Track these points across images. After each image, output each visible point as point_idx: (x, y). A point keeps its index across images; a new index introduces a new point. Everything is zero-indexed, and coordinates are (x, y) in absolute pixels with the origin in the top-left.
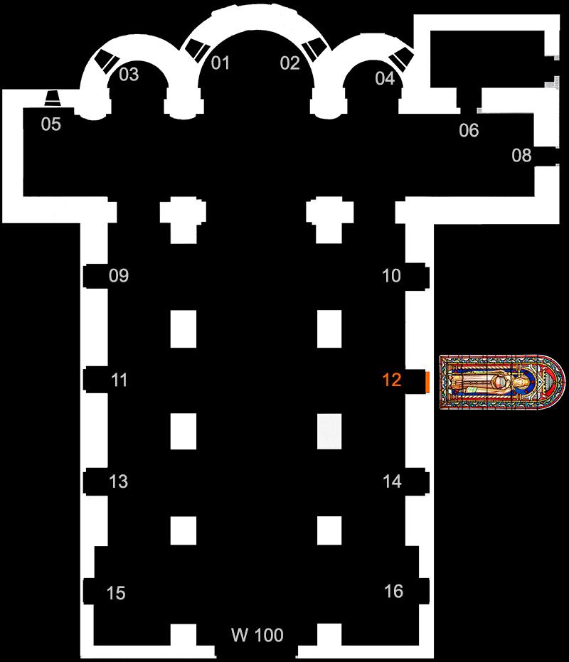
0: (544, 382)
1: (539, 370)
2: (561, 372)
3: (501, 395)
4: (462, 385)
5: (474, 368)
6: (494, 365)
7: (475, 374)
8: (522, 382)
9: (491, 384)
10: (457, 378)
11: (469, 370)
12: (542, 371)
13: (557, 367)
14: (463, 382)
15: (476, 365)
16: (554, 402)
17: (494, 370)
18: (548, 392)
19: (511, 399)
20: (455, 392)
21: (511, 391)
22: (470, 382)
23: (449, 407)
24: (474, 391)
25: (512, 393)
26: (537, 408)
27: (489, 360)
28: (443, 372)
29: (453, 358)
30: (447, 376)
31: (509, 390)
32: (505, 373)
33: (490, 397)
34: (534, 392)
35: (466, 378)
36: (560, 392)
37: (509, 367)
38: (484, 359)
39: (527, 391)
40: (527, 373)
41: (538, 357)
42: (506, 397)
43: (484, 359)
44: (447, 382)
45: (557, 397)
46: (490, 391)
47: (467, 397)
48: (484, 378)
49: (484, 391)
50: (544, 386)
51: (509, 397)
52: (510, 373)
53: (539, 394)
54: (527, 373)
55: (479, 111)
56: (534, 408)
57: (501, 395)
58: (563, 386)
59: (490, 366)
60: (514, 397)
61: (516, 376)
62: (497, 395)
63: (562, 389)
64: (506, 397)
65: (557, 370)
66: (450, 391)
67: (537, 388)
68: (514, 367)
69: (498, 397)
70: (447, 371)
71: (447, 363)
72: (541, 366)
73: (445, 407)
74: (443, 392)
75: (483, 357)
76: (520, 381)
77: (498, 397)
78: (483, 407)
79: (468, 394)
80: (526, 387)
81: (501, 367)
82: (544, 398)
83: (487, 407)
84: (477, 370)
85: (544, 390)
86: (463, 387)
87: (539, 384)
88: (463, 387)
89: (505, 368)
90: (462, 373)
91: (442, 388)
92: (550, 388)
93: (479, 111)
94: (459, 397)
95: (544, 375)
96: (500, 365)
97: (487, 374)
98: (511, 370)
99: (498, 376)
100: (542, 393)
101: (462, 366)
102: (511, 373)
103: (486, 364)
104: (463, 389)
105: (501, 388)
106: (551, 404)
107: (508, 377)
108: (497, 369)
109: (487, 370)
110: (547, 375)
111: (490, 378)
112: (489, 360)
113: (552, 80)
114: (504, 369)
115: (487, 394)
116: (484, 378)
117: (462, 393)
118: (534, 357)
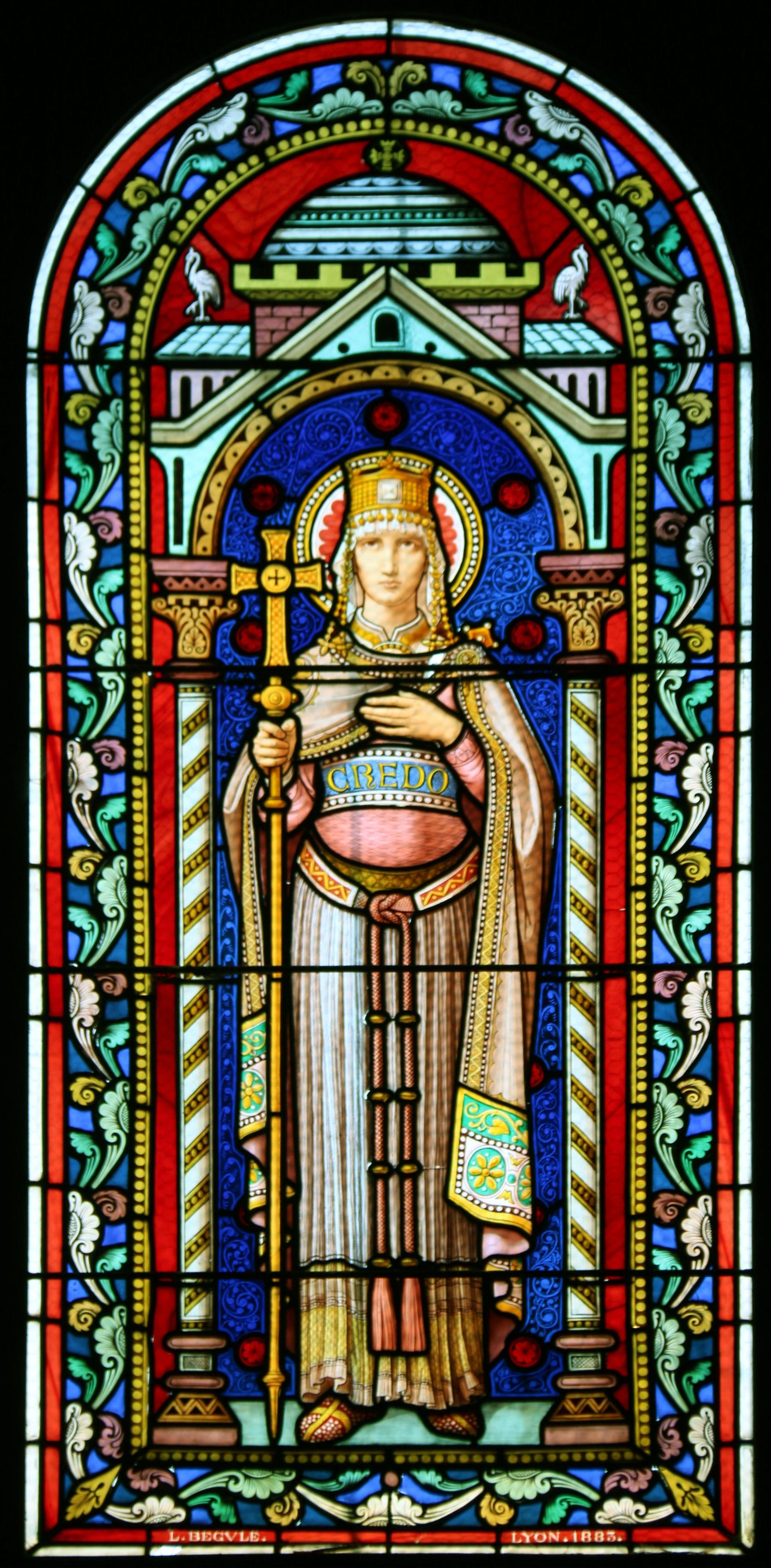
0: (378, 275)
1: (232, 340)
2: (247, 79)
3: (556, 798)
4: (425, 1272)
5: (194, 1128)
6: (163, 881)
7: (288, 1111)
8: (387, 548)
9: (405, 926)
10: (327, 1341)
11: (227, 1150)
12: (229, 308)
13: (188, 122)
14: (385, 1267)
15: (164, 1108)
16: (648, 164)
17: (225, 880)
18: (520, 222)
19: (611, 672)
20: (522, 1360)
21: (499, 670)
22: (390, 1175)
23: (726, 1443)
24: (509, 1127)
25: (530, 659)
26: (722, 355)
27: (93, 940)
28: (250, 1514)
29: (57, 1383)
30: (315, 1460)
31: (496, 708)
32: (265, 746)
33: (578, 930)
34: (522, 401)
35: (337, 1216)
36: (518, 82)
37: (190, 704)
38: (85, 999)
39: (511, 485)
40: (262, 494)
41: (55, 356)
42: (581, 740)
43: (85, 999)
44: (389, 1464)
45: (573, 115)
46: (503, 932)
47: (579, 1214)
48: (332, 1008)
49: (502, 1010)
50: (444, 276)
51: (583, 697)
52: (273, 695)
53: (541, 339)
54: (262, 494)
55: (287, 663)
56: (723, 397)
57: (556, 798)
58: (430, 54)
59: (166, 930)
60: (583, 634)
61: (312, 620)
62: (552, 853)
63: (469, 60)
64: (581, 740)
65: (227, 121)
66: (510, 1424)
67: (468, 363)
68: (193, 645)
69: (579, 836)
70: (240, 1457)
71: (130, 1460)
72: (172, 317)
73: (721, 1488)
74: (528, 1515)
75: (57, 1015)
76: (374, 563)
77: (579, 836)
78: (723, 1022)
79: (547, 1206)
80: (453, 501)
81: (192, 795)
82: (597, 281)
83: (722, 966)
84: (223, 1094)
85: (493, 275)
86: (443, 1270)
87: (416, 337)
88: (443, 1270)
89: (193, 748)
90: (259, 1282)
91: (468, 1523)
92: (469, 208)
93: (256, 697)
94: (578, 1308)
95: (285, 278)
96: (164, 812)
97: (285, 973)
98: (236, 678)
99: (306, 834)
100: (534, 307)
101: (167, 1281)
102: (263, 676)
103: (147, 985)
104: (477, 1269)
105: (469, 806)
106: (673, 198)
107: (324, 712)
108: (217, 851)
109: (221, 974)
110: (298, 238)
111: (330, 933)
112: (93, 940)
113: (471, 1397)
114: (220, 762)
115: (545, 974)
116: (332, 1008)
117: (525, 1271)
118: (54, 398)
